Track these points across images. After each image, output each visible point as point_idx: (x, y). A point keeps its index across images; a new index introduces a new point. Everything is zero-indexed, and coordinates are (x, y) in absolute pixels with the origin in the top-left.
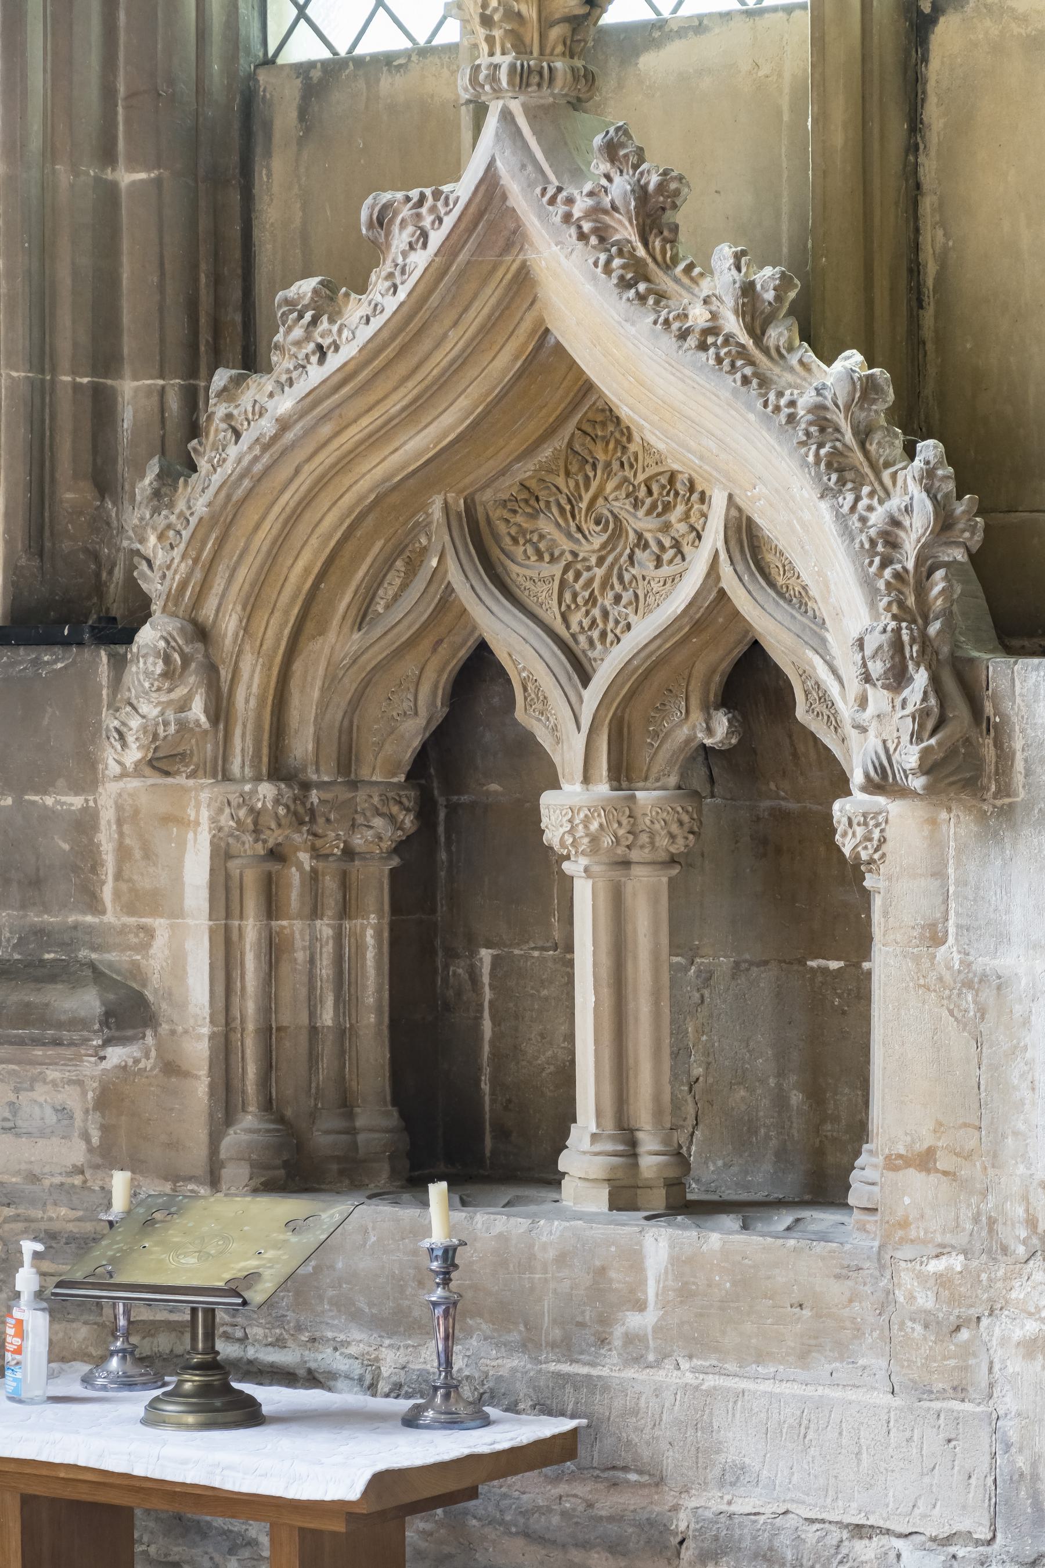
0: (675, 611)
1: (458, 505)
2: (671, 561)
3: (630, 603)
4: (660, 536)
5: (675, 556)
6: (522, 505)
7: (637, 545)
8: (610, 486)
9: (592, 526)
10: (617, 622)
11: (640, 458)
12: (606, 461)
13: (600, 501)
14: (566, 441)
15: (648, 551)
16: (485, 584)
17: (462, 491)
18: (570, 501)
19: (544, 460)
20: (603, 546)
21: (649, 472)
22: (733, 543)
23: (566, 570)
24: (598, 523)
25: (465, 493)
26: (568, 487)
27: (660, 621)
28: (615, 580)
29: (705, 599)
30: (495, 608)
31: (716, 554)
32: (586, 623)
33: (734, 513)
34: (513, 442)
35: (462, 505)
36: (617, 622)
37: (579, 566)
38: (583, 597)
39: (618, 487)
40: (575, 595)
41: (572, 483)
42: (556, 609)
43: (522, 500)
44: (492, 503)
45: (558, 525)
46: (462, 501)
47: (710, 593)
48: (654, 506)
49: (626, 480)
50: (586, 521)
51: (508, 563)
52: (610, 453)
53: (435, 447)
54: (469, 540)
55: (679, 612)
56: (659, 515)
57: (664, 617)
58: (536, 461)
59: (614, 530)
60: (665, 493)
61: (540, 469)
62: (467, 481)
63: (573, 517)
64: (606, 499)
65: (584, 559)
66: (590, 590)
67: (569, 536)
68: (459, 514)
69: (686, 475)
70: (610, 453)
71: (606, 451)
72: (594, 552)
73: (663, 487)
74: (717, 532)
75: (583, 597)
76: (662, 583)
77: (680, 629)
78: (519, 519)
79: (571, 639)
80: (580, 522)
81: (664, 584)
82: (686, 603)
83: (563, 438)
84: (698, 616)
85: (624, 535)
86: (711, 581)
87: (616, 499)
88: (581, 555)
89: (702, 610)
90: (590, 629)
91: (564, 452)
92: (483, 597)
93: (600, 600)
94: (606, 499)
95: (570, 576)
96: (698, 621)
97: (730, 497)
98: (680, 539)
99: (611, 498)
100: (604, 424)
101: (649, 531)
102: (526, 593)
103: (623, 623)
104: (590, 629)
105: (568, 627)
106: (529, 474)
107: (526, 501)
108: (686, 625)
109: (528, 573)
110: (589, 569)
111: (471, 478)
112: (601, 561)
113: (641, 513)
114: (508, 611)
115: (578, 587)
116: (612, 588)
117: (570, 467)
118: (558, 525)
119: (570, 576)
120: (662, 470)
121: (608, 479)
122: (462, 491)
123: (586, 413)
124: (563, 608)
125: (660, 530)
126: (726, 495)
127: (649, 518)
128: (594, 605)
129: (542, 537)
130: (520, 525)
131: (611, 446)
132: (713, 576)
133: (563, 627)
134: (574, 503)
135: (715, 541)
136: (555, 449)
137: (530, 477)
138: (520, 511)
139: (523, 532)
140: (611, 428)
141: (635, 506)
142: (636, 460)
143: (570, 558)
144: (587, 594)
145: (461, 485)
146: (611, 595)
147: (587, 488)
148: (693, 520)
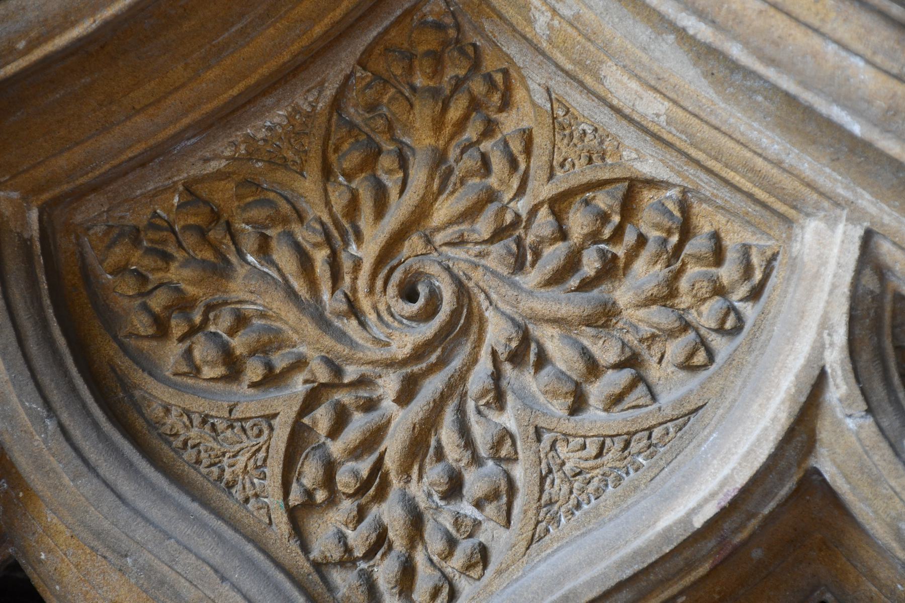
0: (686, 520)
1: (25, 224)
2: (615, 400)
3: (494, 495)
4: (586, 337)
5: (631, 386)
6: (189, 240)
7: (517, 358)
8: (443, 211)
9: (391, 297)
10: (452, 543)
11: (541, 140)
12: (435, 150)
13: (413, 244)
14: (330, 92)
15: (547, 370)
16: (96, 425)
17: (39, 189)
18: (328, 239)
19: (261, 135)
20: (419, 353)
21: (563, 182)
22: (865, 357)
23: (310, 402)
24: (410, 295)
25: (45, 196)
26: (328, 204)
27: (638, 543)
28: (447, 435)
29: (768, 495)
30: (127, 488)
31: (820, 381)
32: (358, 539)
33: (870, 282)
34: (210, 75)
35: (35, 226)
36: (452, 543)
37: (345, 397)
38: (356, 474)
39: (471, 214)
40: (330, 468)
41: (339, 200)
42: (274, 499)
43: (186, 228)
44: (100, 229)
45: (291, 294)
46: (34, 215)
47: (781, 481)
48: (572, 263)
49: (491, 196)
50: (371, 290)
51: (139, 377)
52: (448, 130)
53: (28, 50)
54: (50, 312)
55: (698, 522)
56: (586, 285)
57: (650, 534)
58: (238, 136)
59: (455, 314)
60: (607, 232)
61: (250, 156)
62: (62, 162)
63: (336, 277)
64: (428, 241)
65: (362, 382)
66: (375, 456)
67: (322, 322)
68: (26, 245)
69: (674, 193)
70: (448, 130)
71: (438, 124)
72: (391, 364)
73: (604, 218)
74: (825, 325)
75: (356, 474)
76: (592, 450)
77: (690, 566)
78: (176, 273)
79: (315, 577)
80: (354, 290)
81: (599, 455)
82: (722, 500)
83: (321, 86)
84: (738, 539)
85: (475, 328)
86: (791, 452)
87: (460, 242)
88: (351, 373)
89: (753, 524)
90: (370, 554)
91: (322, 120)
92: (92, 457)
93: (396, 483)
94: (428, 241)
95: (322, 418)
96: (737, 549)
97: (868, 238)
98: (642, 349)
99: (439, 238)
100: (437, 59)
101: (556, 321)
102: (189, 455)
103: (465, 547)
104: (370, 554)
105: (305, 548)
106: (214, 166)
107: (202, 232)
108: (704, 558)
109: (198, 405)
110: (370, 405)
111: (78, 154)
112: (405, 396)
113: (532, 278)
114: (165, 498)
115: (336, 448)
116: (440, 455)
117: (333, 157)
118: (291, 294)
119: (322, 418)
120: (606, 175)
121: (441, 191)
122: (39, 189)
123: (386, 31)
124: (295, 498)
125: (589, 322)
126: (859, 232)
127: (556, 291)
128: (381, 495)
129: (241, 321)
130: (178, 290)
131: (454, 114)
132: (799, 439)
133: (294, 546)
134: (339, 243)
135: (819, 348)
136: (296, 110)
137: (220, 175)
138: (179, 255)
139: (183, 305)
140: (453, 71)
141: (519, 265)
142: (528, 150)
143: (323, 376)
144: (364, 467)
145: (41, 173)
146: (435, 473)
147: (380, 209)
148: (684, 301)
